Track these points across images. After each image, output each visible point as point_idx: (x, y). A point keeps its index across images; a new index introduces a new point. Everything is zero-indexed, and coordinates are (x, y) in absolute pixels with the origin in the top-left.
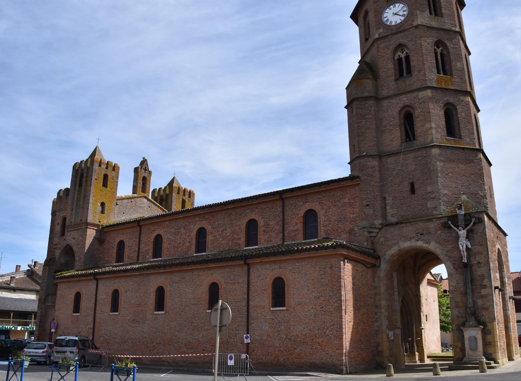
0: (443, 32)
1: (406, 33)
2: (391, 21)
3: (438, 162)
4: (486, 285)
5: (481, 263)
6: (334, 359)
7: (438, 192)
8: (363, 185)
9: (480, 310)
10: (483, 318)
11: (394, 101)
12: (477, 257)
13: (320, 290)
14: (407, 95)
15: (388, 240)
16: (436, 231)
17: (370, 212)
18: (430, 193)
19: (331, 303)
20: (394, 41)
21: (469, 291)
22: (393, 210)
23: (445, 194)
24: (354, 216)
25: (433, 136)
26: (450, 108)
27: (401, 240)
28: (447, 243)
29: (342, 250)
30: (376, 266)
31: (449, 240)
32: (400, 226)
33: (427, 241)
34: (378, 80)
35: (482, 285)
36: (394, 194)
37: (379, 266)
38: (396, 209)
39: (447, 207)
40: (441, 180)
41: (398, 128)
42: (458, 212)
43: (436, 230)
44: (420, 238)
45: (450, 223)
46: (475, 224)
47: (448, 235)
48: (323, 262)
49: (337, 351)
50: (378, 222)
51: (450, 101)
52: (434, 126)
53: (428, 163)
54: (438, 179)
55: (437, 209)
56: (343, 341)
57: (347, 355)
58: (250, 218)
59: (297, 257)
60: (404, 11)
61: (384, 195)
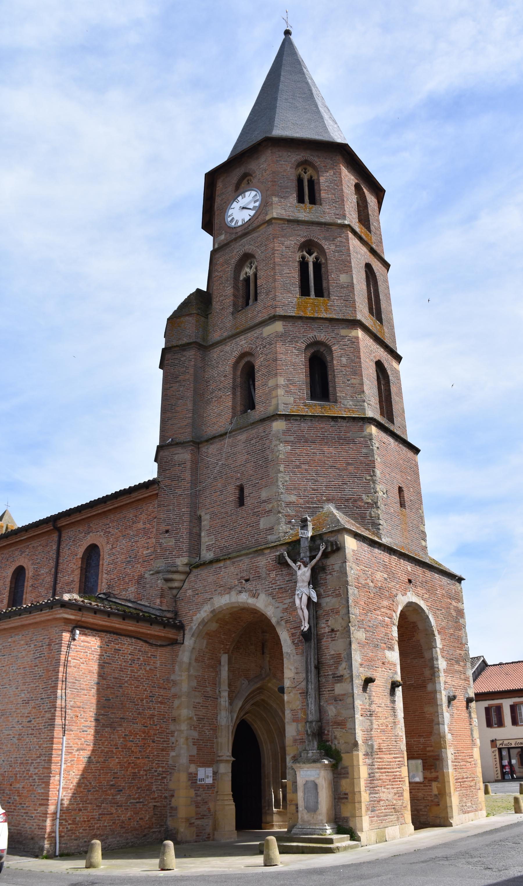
0: (319, 228)
1: (255, 235)
2: (237, 220)
3: (281, 444)
4: (342, 676)
5: (336, 631)
6: (35, 824)
7: (276, 500)
9: (331, 725)
10: (336, 743)
11: (227, 348)
12: (331, 618)
13: (31, 687)
14: (246, 335)
15: (198, 594)
16: (268, 573)
17: (170, 544)
18: (264, 501)
19: (41, 712)
20: (238, 250)
21: (312, 687)
24: (149, 551)
26: (321, 350)
28: (285, 595)
29: (61, 611)
30: (179, 642)
31: (288, 588)
34: (209, 316)
35: (336, 675)
36: (213, 509)
37: (182, 642)
40: (283, 477)
41: (229, 393)
42: (301, 533)
45: (286, 555)
46: (326, 555)
47: (287, 578)
48: (41, 634)
49: (39, 809)
50: (182, 561)
51: (319, 339)
52: (283, 383)
56: (49, 788)
57: (58, 816)
58: (18, 564)
59: (6, 627)
60: (255, 202)
61: (199, 513)
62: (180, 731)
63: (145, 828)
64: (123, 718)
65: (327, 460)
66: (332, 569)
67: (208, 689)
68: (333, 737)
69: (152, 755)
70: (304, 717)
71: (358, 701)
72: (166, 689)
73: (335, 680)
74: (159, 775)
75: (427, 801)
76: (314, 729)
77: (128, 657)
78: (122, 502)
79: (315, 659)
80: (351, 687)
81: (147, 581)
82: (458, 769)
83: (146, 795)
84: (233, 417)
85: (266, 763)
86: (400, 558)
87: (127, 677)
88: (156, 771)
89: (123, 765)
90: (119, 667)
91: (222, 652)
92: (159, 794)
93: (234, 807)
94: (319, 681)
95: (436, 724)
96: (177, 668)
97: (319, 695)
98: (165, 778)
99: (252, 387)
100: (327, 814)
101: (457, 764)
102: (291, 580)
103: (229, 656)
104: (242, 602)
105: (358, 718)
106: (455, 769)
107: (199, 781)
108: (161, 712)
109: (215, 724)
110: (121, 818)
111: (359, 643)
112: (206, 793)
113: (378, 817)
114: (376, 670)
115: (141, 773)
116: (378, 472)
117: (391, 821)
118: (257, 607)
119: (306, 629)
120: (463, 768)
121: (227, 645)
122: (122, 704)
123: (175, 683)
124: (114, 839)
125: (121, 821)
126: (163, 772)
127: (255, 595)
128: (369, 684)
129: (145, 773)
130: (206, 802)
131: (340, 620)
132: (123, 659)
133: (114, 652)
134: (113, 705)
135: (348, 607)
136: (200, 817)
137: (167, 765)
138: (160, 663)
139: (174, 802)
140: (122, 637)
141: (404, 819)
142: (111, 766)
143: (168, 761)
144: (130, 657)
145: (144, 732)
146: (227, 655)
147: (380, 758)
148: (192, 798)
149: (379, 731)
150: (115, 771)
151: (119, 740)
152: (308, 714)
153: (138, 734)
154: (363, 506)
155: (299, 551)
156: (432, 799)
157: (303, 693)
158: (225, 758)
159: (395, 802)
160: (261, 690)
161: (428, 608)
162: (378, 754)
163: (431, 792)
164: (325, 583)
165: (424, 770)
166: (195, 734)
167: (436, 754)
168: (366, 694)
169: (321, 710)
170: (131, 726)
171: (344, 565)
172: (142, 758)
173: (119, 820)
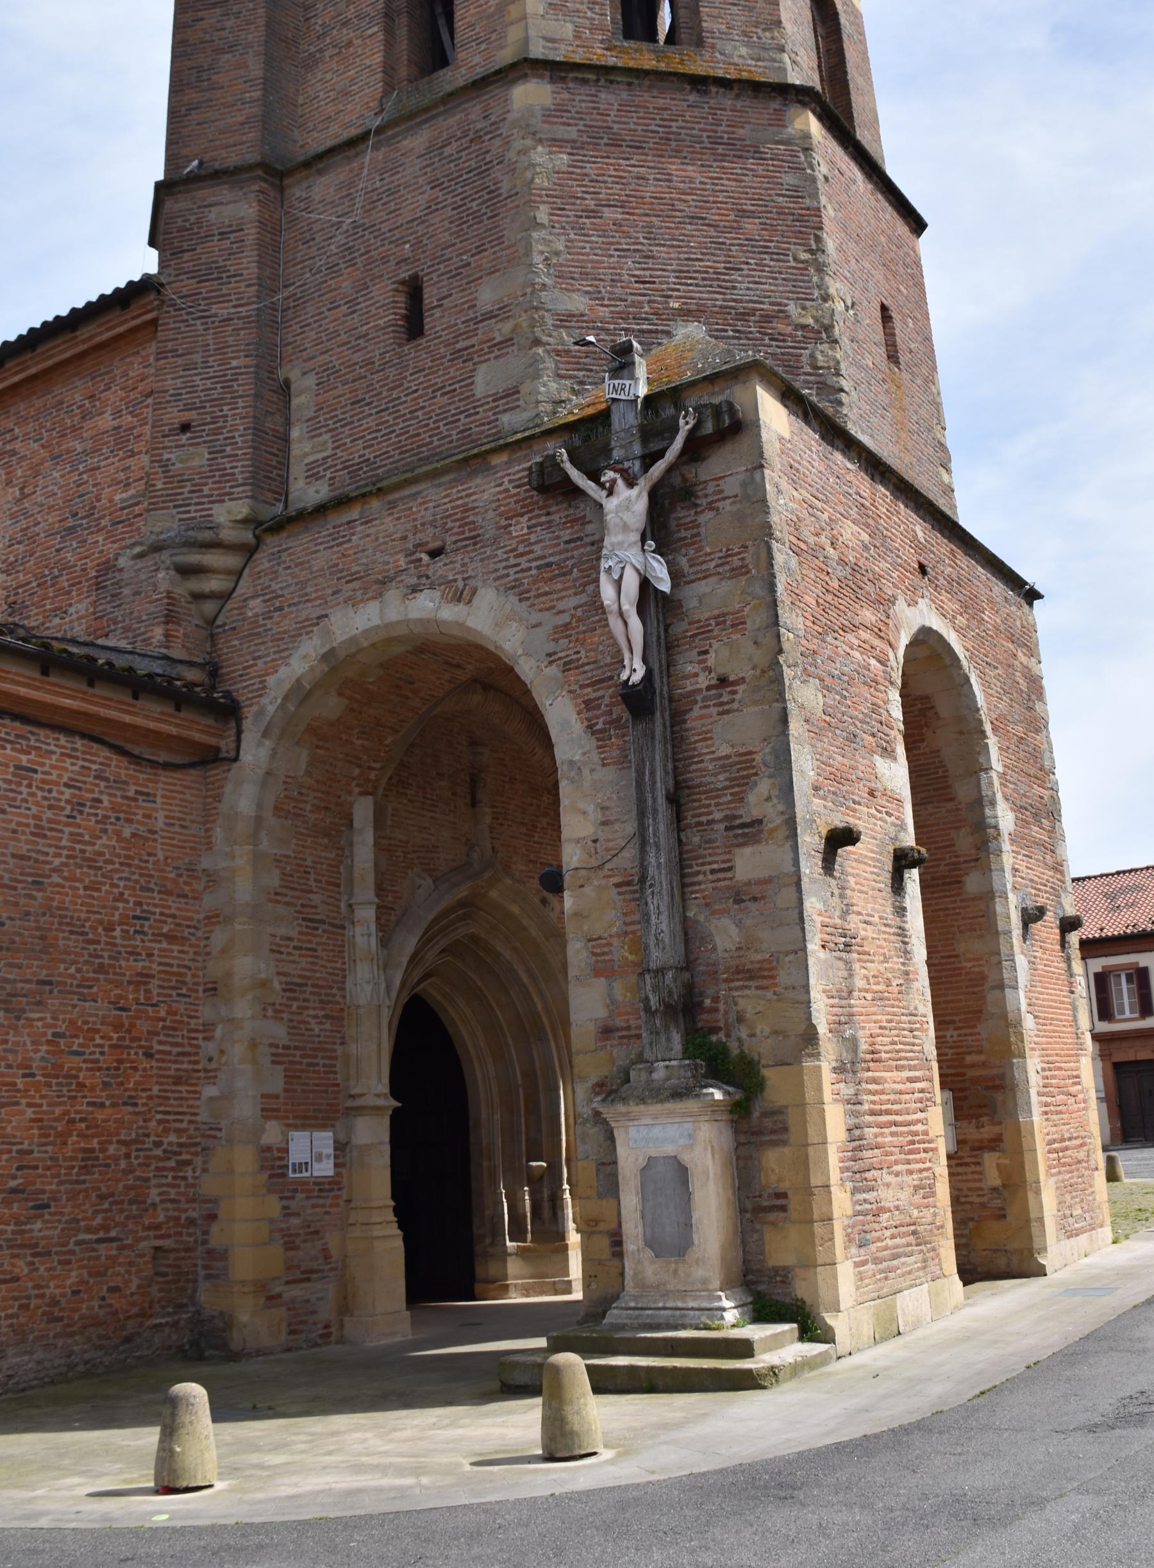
3: (540, 148)
4: (760, 822)
8: (172, 326)
9: (726, 980)
10: (744, 1036)
12: (716, 645)
15: (281, 609)
16: (503, 523)
18: (489, 316)
21: (659, 863)
22: (316, 439)
23: (573, 316)
24: (132, 492)
25: (526, 29)
27: (341, 599)
28: (559, 586)
30: (222, 755)
31: (570, 563)
32: (338, 522)
33: (457, 589)
35: (738, 822)
37: (233, 754)
38: (329, 434)
39: (576, 387)
40: (547, 242)
41: (375, 29)
43: (506, 519)
44: (428, 577)
45: (565, 456)
46: (696, 448)
53: (491, 161)
54: (535, 235)
55: (518, 400)
61: (281, 374)
62: (231, 1021)
63: (129, 1318)
64: (50, 983)
65: (680, 200)
66: (715, 493)
67: (316, 899)
68: (732, 1016)
69: (144, 1095)
70: (631, 957)
71: (814, 899)
72: (185, 896)
73: (736, 836)
74: (168, 1154)
75: (968, 1207)
76: (670, 993)
77: (62, 793)
78: (52, 357)
79: (667, 773)
80: (790, 855)
81: (126, 576)
82: (1052, 1112)
83: (127, 1217)
84: (386, 94)
85: (484, 1116)
86: (897, 498)
87: (58, 855)
88: (158, 1144)
89: (51, 1127)
90: (32, 822)
91: (356, 790)
92: (171, 1213)
93: (399, 1243)
94: (680, 841)
95: (993, 988)
96: (218, 833)
97: (683, 886)
98: (188, 1163)
99: (442, 22)
100: (723, 1259)
101: (1049, 1100)
102: (580, 539)
103: (375, 803)
104: (420, 621)
105: (814, 952)
106: (1046, 1113)
107: (294, 1171)
108: (171, 965)
109: (338, 1003)
110: (48, 1292)
111: (807, 721)
112: (314, 1206)
113: (876, 1261)
114: (854, 810)
115: (112, 1149)
116: (830, 245)
117: (910, 1273)
118: (469, 629)
119: (637, 678)
120: (1061, 1112)
121: (371, 768)
122: (43, 938)
123: (212, 879)
124: (26, 1358)
125: (47, 1300)
126: (180, 1145)
127: (461, 595)
128: (839, 851)
129: (123, 1150)
130: (317, 1232)
131: (748, 648)
132: (45, 798)
133: (14, 775)
134: (13, 942)
135: (774, 603)
136: (299, 1276)
137: (192, 1127)
138: (166, 817)
139: (217, 1238)
140: (42, 733)
141: (940, 1264)
142: (9, 1130)
143: (195, 1114)
144: (68, 793)
145: (118, 1027)
146: (370, 799)
147: (875, 1081)
148: (272, 1221)
149: (869, 996)
150: (25, 1147)
151: (36, 1051)
152: (647, 947)
153: (98, 1031)
154: (790, 335)
155: (609, 444)
156: (985, 1199)
157: (629, 883)
158: (370, 1101)
159: (915, 1213)
160: (467, 908)
161: (967, 654)
162: (868, 1070)
163: (980, 1180)
164: (693, 536)
165: (956, 1119)
166: (279, 1032)
167: (995, 1071)
168: (833, 882)
169: (688, 933)
170: (74, 1006)
171: (757, 475)
172: (113, 1105)
173: (43, 1296)
